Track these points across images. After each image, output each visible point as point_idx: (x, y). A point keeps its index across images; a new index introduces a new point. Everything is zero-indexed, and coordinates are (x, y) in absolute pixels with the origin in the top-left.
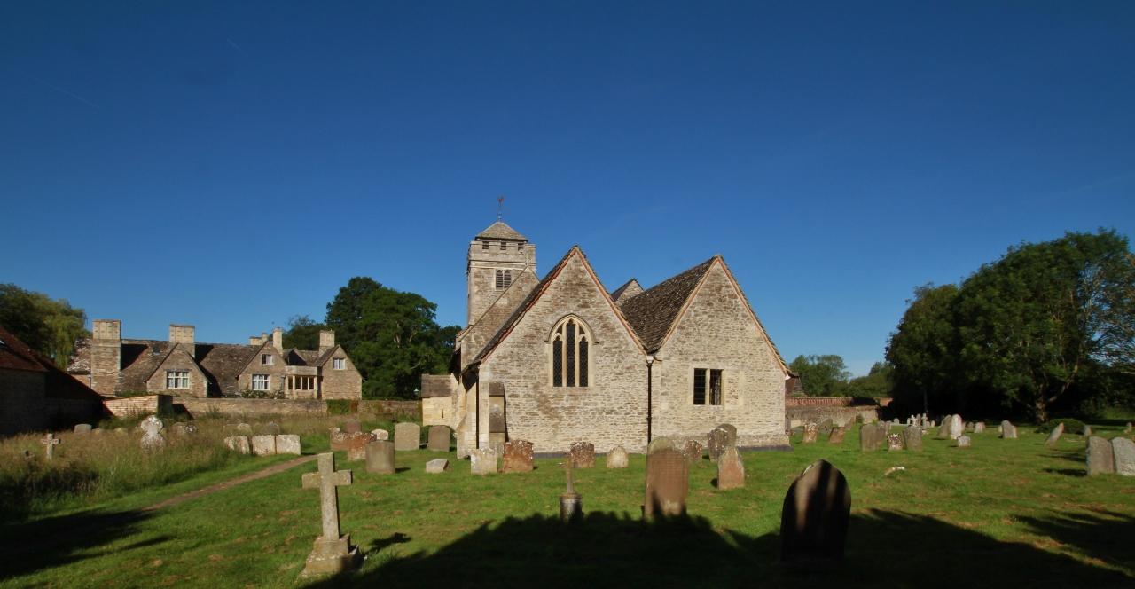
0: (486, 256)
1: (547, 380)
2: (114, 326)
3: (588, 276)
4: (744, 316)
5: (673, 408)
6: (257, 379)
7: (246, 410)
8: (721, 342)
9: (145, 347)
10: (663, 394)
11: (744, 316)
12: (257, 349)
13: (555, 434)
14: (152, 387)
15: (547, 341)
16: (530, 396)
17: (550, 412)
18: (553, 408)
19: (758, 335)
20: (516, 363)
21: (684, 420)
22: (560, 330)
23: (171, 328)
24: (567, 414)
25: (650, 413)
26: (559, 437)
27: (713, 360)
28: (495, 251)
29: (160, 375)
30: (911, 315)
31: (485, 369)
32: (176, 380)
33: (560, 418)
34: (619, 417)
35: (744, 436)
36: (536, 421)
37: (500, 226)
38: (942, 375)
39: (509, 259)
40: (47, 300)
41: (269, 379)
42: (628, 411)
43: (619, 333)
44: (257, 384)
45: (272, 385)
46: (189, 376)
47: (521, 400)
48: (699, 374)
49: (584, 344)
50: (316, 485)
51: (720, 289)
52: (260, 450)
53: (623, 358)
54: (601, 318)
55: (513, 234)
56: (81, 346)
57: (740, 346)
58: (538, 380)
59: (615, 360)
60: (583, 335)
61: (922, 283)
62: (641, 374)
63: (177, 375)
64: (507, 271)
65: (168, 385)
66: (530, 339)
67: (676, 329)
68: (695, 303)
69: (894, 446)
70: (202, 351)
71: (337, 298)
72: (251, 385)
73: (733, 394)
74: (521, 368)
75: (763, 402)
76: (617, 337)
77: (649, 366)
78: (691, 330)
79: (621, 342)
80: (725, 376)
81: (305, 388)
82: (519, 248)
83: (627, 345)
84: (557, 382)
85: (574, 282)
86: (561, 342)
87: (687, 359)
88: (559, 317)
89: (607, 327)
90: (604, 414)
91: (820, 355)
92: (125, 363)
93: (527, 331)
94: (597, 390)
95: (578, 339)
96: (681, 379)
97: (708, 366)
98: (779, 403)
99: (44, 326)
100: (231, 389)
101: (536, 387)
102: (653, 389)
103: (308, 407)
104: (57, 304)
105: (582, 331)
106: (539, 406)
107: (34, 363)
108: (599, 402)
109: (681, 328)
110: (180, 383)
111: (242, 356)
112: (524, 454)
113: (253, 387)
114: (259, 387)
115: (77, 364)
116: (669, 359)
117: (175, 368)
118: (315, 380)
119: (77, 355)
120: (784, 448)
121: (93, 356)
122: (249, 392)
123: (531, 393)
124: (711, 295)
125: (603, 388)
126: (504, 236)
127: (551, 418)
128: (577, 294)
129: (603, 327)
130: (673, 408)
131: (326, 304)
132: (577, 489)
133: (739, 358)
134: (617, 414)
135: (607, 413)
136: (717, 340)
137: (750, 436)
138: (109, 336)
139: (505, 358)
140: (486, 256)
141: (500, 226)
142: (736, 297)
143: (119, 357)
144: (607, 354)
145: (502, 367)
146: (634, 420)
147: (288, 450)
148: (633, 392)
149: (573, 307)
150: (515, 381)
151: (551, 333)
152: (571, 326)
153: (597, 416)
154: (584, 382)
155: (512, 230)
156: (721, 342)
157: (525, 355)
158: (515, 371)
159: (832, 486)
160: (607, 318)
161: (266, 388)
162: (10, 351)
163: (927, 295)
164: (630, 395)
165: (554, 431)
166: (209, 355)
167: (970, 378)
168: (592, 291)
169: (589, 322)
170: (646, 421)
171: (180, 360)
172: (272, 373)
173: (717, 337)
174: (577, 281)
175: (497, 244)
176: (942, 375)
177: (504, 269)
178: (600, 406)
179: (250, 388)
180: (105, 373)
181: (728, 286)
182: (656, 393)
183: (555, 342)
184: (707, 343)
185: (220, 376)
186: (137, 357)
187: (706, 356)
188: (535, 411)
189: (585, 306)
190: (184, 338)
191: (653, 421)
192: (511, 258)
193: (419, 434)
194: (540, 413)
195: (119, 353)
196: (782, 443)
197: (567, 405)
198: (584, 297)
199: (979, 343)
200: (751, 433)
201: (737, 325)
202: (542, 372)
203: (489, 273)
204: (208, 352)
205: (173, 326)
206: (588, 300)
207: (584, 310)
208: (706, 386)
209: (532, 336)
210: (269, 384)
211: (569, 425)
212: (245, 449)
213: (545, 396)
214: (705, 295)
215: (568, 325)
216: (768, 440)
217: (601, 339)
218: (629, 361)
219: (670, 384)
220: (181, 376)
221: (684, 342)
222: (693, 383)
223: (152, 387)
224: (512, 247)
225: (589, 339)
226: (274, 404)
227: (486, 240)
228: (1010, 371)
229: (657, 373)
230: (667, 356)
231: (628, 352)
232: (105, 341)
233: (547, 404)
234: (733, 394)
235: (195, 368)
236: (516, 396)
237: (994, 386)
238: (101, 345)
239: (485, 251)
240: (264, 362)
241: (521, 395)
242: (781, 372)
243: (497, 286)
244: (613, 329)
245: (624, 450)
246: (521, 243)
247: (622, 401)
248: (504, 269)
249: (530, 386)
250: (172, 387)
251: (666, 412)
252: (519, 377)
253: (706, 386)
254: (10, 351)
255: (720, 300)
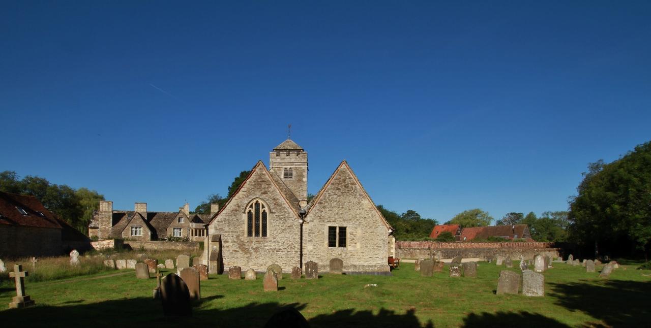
0: (279, 160)
1: (244, 233)
2: (109, 204)
3: (267, 177)
4: (360, 195)
5: (315, 249)
6: (176, 231)
7: (159, 248)
8: (346, 211)
9: (124, 214)
10: (309, 241)
11: (360, 195)
12: (175, 215)
13: (248, 262)
14: (124, 235)
15: (244, 213)
16: (235, 242)
17: (246, 251)
18: (247, 248)
19: (370, 206)
20: (227, 224)
21: (322, 256)
22: (251, 206)
23: (136, 205)
24: (254, 251)
25: (301, 252)
26: (250, 264)
27: (340, 221)
28: (283, 157)
29: (128, 229)
30: (585, 187)
31: (211, 228)
32: (136, 231)
33: (251, 254)
34: (284, 253)
35: (360, 266)
36: (238, 255)
37: (288, 142)
38: (596, 226)
39: (292, 161)
40: (87, 191)
41: (182, 231)
42: (289, 250)
43: (284, 208)
44: (176, 233)
45: (183, 234)
46: (142, 229)
47: (230, 244)
48: (332, 230)
49: (264, 214)
50: (14, 276)
51: (345, 180)
52: (119, 267)
53: (286, 221)
54: (274, 199)
55: (295, 147)
56: (96, 214)
57: (358, 213)
58: (239, 233)
59: (282, 222)
60: (263, 209)
61: (594, 160)
62: (296, 230)
63: (136, 229)
64: (290, 168)
65: (132, 234)
66: (235, 212)
67: (317, 204)
68: (329, 189)
69: (454, 274)
70: (151, 215)
71: (233, 183)
72: (172, 234)
73: (353, 241)
74: (230, 227)
75: (373, 246)
76: (283, 209)
77: (301, 225)
78: (326, 204)
79: (285, 212)
80: (348, 231)
81: (200, 235)
82: (298, 155)
83: (289, 214)
84: (250, 234)
85: (259, 180)
86: (266, 213)
87: (323, 221)
88: (250, 199)
89: (277, 204)
90: (275, 252)
91: (553, 211)
92: (114, 223)
93: (233, 207)
94: (271, 239)
95: (261, 211)
96: (320, 232)
97: (337, 225)
98: (384, 247)
99: (79, 205)
100: (163, 236)
101: (238, 237)
102: (303, 238)
103: (189, 246)
104: (91, 193)
105: (263, 207)
106: (239, 247)
107: (53, 223)
108: (272, 245)
109: (320, 203)
110: (138, 232)
111: (169, 218)
112: (203, 271)
113: (174, 235)
114: (177, 235)
115: (93, 223)
116: (313, 221)
117: (135, 225)
118: (205, 231)
119: (93, 219)
120: (386, 273)
121: (100, 220)
122: (171, 237)
123: (235, 240)
124: (338, 184)
125: (275, 238)
126: (289, 148)
127: (245, 253)
128: (261, 187)
129: (275, 204)
130: (315, 249)
131: (228, 187)
132: (361, 302)
133: (357, 220)
134: (282, 251)
135: (277, 251)
136: (343, 209)
137: (364, 266)
138: (107, 209)
139: (221, 222)
140: (279, 160)
141: (288, 142)
142: (355, 184)
143: (111, 220)
144: (277, 219)
145: (220, 227)
146: (292, 255)
147: (132, 267)
148: (292, 240)
149: (258, 194)
150: (227, 234)
151: (246, 208)
152: (257, 204)
153: (271, 252)
154: (264, 234)
155: (294, 144)
156: (346, 211)
157: (232, 220)
158: (227, 229)
159: (174, 281)
160: (278, 199)
161: (180, 235)
162: (47, 219)
163: (595, 167)
164: (290, 241)
165: (247, 260)
166: (154, 218)
167: (614, 229)
168: (270, 184)
169: (267, 202)
170: (299, 256)
171: (138, 221)
172: (183, 227)
173: (343, 208)
174: (261, 180)
175: (284, 153)
176: (596, 226)
177: (288, 167)
178: (273, 247)
179: (172, 236)
180: (105, 228)
181: (350, 178)
182: (306, 240)
183: (248, 213)
184: (337, 211)
185: (158, 229)
186: (120, 219)
187: (336, 219)
188: (237, 250)
189: (265, 193)
190: (141, 209)
191: (304, 256)
192: (293, 160)
193: (189, 260)
194: (240, 251)
195: (111, 218)
196: (385, 270)
197: (255, 247)
198: (264, 188)
199: (619, 204)
200: (366, 264)
201: (356, 201)
202: (241, 229)
203: (280, 170)
204: (153, 217)
205: (136, 203)
206: (267, 190)
207: (265, 196)
208: (338, 237)
209: (236, 210)
210: (182, 233)
211: (256, 257)
212: (113, 266)
213: (243, 242)
214: (336, 184)
215: (255, 204)
216: (376, 268)
217: (274, 211)
218: (290, 222)
219: (314, 235)
220: (138, 229)
221: (322, 211)
222: (328, 235)
223: (124, 235)
224: (293, 154)
225: (267, 211)
226: (172, 244)
227: (278, 151)
228: (641, 224)
229: (306, 229)
230: (311, 220)
231: (289, 217)
232: (105, 212)
233: (244, 246)
234: (353, 241)
235: (145, 225)
236: (227, 242)
237: (630, 235)
238: (103, 214)
239: (287, 157)
240: (179, 221)
241: (230, 241)
242: (386, 228)
243: (284, 177)
244: (281, 205)
245: (253, 270)
246: (298, 151)
247: (285, 245)
248: (288, 167)
249: (235, 236)
250: (134, 235)
251: (311, 251)
252: (229, 232)
253: (338, 237)
254: (47, 219)
255: (345, 186)
